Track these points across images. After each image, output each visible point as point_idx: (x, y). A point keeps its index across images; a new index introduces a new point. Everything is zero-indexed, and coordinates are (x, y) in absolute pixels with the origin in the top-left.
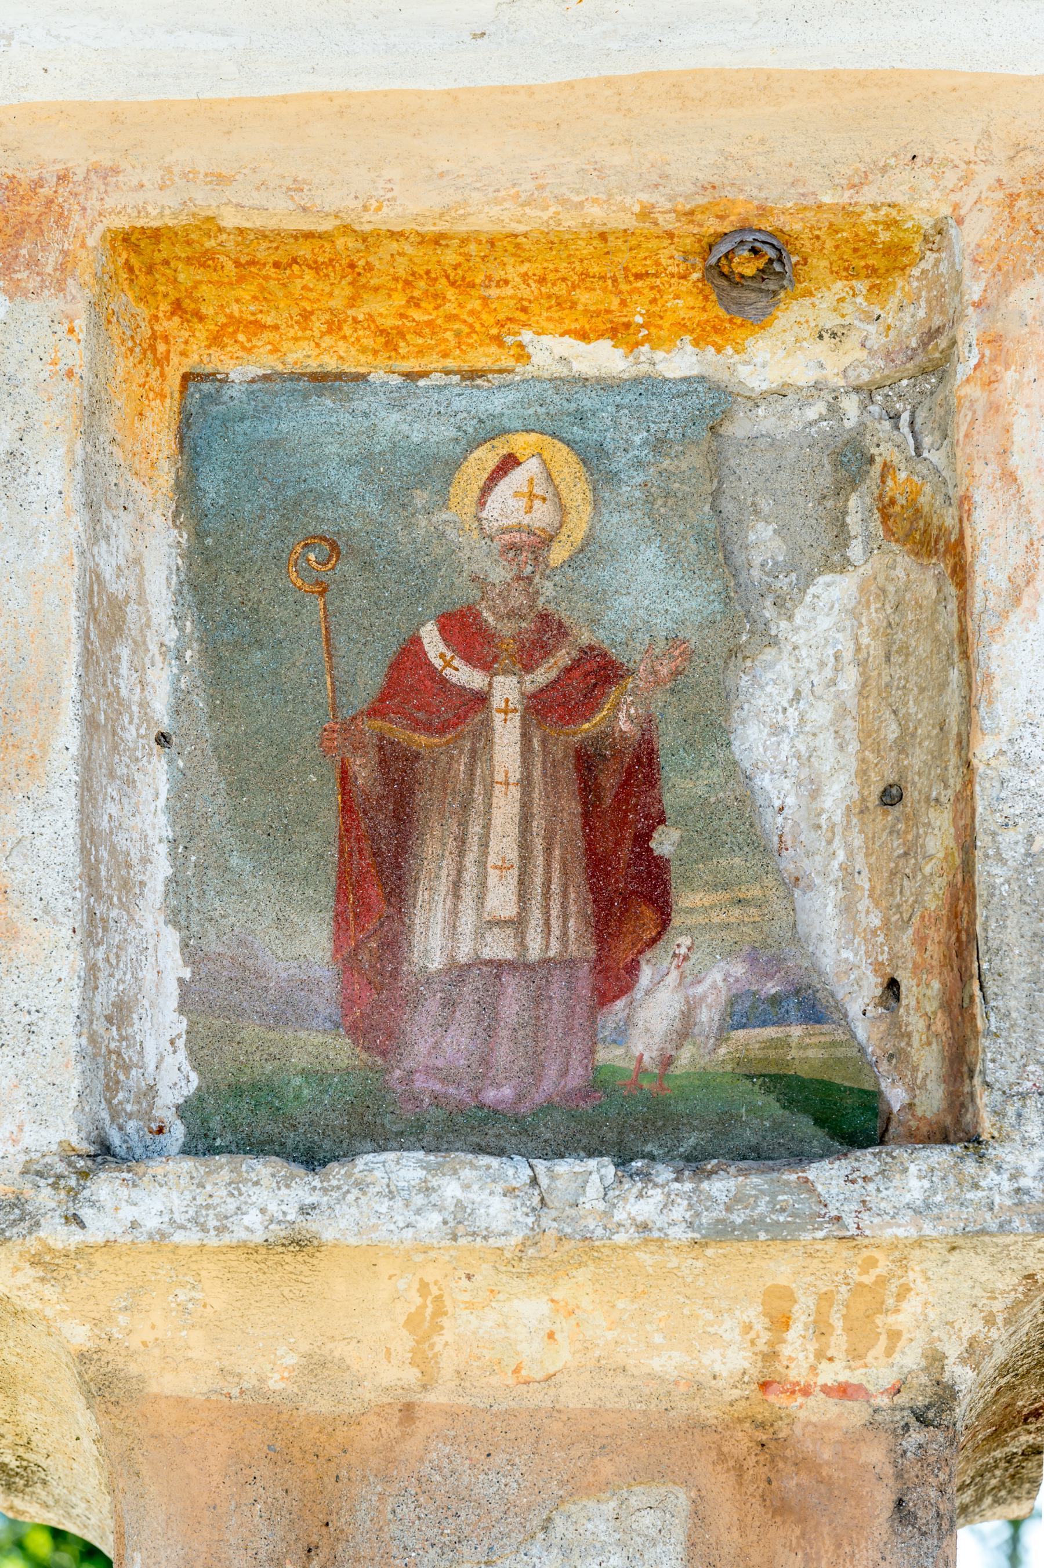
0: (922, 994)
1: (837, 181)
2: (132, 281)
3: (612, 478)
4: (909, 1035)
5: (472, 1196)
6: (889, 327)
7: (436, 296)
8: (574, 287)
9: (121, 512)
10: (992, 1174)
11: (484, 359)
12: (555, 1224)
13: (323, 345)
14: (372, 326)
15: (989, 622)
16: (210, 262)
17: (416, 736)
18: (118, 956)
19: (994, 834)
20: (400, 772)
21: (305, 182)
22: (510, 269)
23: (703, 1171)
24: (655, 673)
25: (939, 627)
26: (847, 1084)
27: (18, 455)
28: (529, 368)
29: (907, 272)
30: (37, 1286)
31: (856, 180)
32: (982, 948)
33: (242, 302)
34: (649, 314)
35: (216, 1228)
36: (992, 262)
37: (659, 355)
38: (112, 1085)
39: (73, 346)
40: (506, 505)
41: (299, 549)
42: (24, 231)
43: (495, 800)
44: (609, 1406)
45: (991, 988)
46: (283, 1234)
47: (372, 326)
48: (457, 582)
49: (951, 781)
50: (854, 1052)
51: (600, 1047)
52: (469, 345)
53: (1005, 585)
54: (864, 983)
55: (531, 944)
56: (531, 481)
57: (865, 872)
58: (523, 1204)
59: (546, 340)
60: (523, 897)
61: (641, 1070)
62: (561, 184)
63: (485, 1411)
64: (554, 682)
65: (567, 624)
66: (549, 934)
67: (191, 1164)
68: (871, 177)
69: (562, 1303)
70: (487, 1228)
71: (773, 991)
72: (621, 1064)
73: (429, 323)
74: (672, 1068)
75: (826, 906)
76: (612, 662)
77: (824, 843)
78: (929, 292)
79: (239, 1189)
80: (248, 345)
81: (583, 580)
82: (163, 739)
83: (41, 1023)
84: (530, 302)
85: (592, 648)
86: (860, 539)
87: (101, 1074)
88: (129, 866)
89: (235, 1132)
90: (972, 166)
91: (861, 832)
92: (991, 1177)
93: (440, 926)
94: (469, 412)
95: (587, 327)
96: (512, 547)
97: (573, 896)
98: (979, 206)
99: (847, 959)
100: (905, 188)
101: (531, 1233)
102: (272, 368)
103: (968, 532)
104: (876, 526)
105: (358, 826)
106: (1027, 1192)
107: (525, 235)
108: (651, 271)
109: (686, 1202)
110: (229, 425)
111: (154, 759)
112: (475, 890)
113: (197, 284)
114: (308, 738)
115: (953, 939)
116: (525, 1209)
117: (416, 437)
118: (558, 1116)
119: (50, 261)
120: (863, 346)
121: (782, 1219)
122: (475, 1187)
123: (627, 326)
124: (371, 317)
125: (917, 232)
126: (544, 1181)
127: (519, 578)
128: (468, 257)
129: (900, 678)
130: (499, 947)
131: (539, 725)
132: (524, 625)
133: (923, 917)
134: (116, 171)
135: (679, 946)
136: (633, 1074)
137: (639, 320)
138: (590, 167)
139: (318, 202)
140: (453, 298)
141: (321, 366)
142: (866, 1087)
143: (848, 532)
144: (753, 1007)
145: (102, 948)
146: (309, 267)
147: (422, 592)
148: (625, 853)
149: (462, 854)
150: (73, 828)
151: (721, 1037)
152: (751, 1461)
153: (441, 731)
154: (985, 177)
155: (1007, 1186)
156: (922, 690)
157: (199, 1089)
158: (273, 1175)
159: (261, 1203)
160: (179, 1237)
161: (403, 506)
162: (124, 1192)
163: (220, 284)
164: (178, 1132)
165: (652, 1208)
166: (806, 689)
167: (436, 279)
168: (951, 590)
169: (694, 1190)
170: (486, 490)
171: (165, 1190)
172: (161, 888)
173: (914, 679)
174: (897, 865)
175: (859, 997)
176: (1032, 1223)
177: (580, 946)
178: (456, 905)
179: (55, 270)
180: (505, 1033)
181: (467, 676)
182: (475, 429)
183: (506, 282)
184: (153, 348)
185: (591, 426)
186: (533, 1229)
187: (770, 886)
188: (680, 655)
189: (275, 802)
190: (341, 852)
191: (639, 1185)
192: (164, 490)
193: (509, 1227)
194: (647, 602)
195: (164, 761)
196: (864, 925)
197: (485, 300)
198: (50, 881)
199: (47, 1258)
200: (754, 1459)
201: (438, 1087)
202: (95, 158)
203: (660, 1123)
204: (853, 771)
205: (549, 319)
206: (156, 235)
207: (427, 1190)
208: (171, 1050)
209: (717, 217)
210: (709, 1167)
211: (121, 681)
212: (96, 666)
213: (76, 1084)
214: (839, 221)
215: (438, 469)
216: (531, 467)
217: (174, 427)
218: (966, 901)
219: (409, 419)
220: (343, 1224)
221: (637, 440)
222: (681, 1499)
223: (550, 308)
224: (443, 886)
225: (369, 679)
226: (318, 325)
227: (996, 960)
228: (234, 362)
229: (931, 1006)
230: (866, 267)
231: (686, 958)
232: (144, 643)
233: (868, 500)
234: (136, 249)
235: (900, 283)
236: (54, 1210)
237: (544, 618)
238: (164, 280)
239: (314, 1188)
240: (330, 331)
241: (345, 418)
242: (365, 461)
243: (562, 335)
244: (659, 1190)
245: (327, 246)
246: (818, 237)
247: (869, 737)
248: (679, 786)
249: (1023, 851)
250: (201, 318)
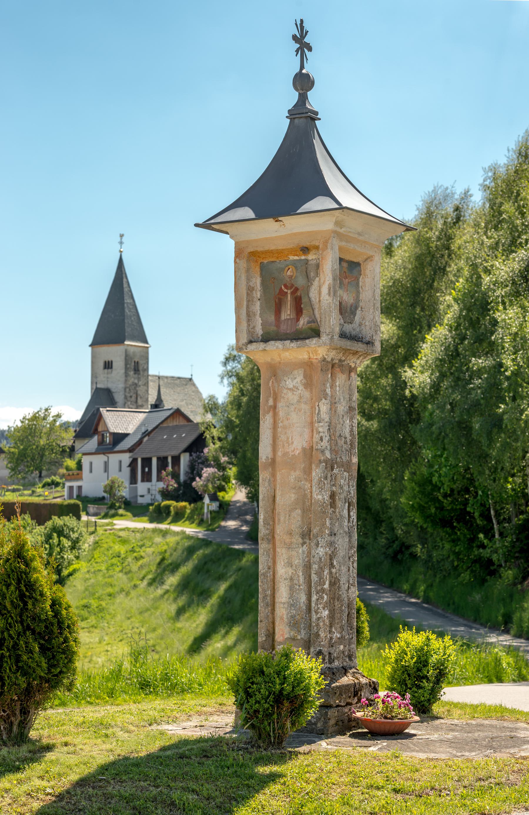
20: (280, 300)
40: (289, 273)
130: (288, 317)
177: (295, 317)
181: (286, 290)
215: (283, 270)
225: (278, 291)
248: (304, 300)
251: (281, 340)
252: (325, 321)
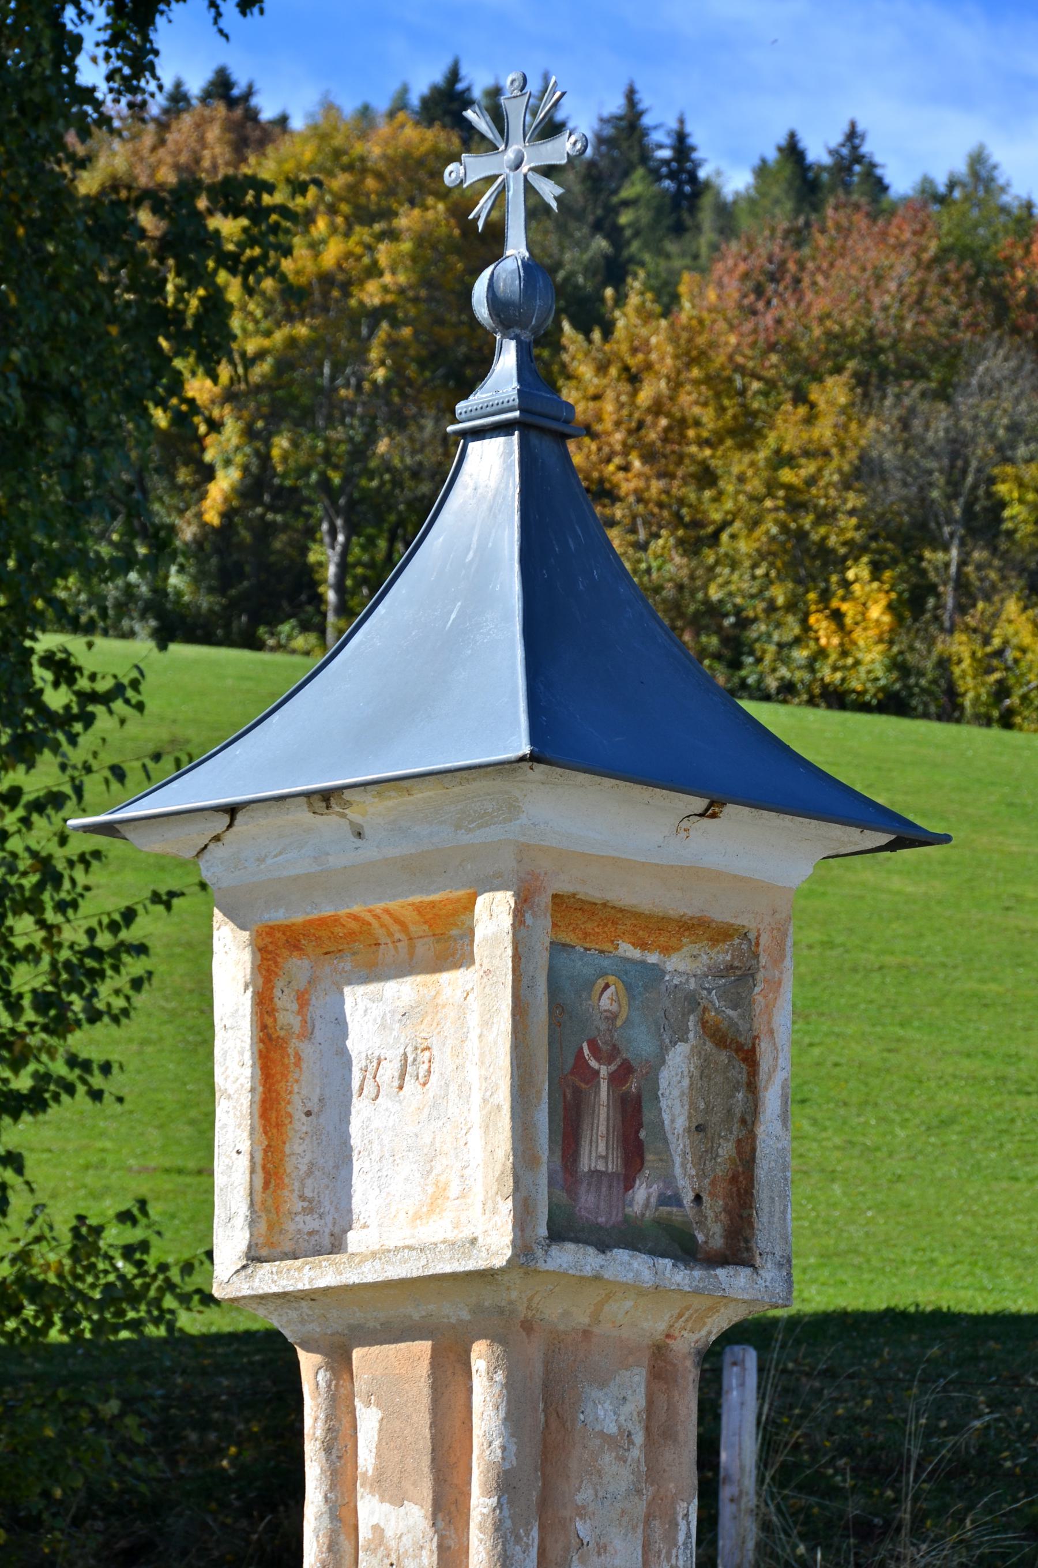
104: (699, 1028)
130: (601, 1167)
177: (620, 1170)
216: (612, 989)
225: (571, 1061)
247: (692, 1105)
248: (647, 1116)
252: (772, 1215)
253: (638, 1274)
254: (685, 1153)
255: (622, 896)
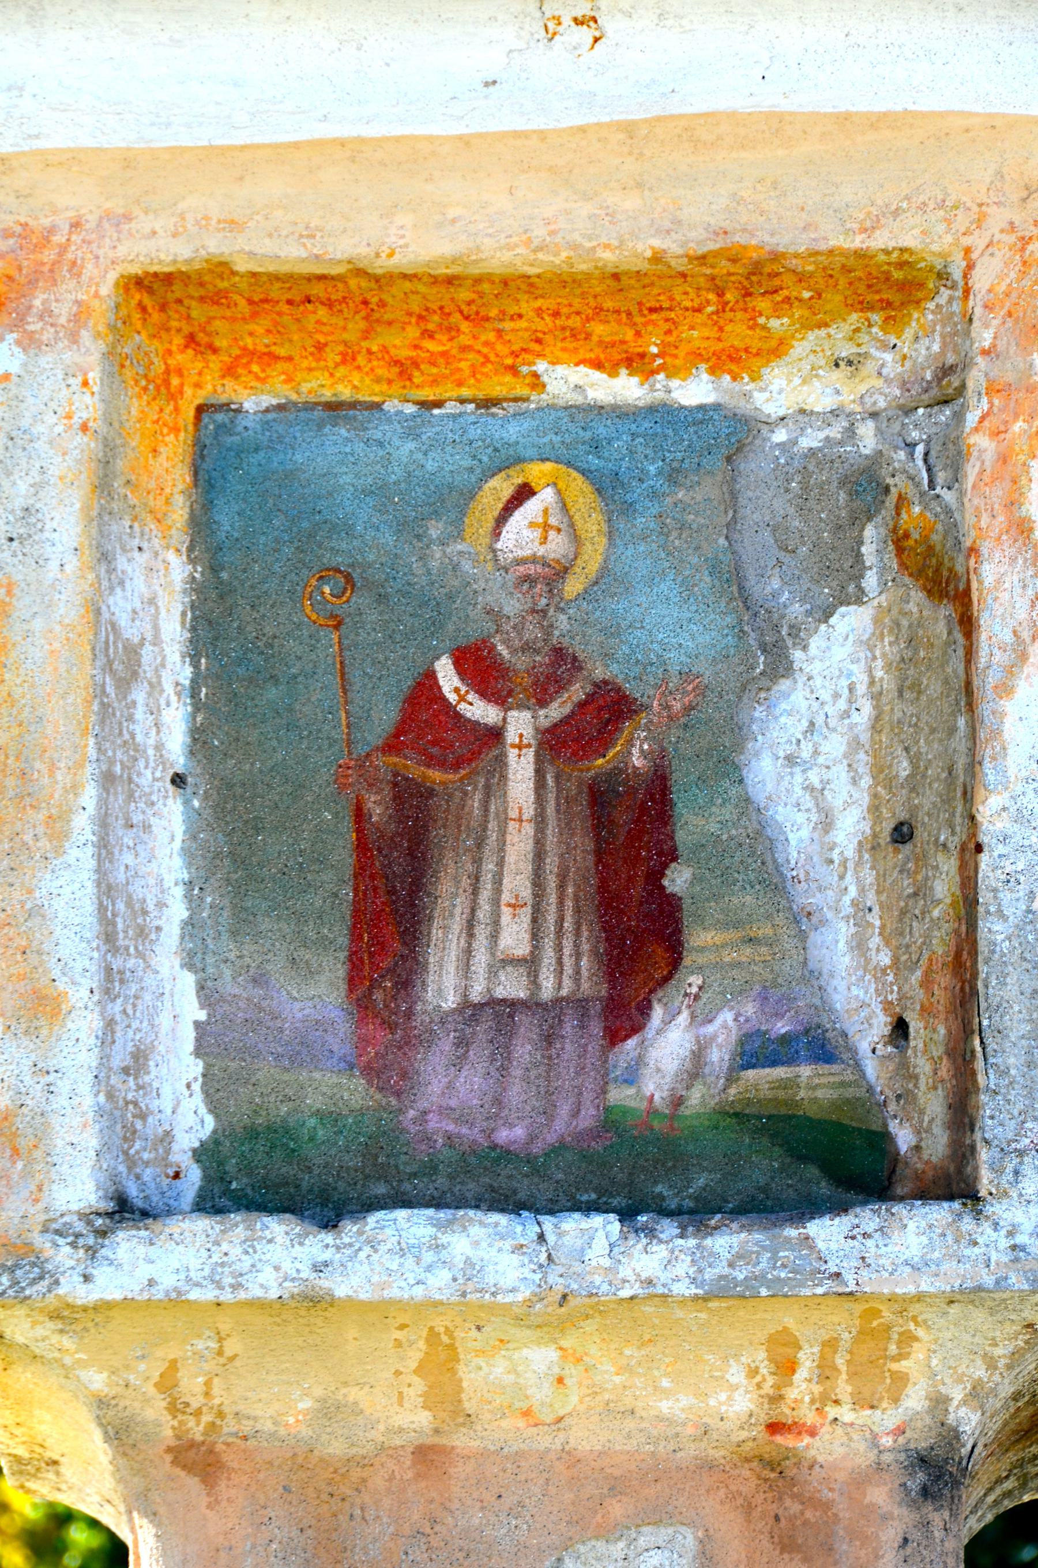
0: (928, 1037)
1: (848, 226)
2: (145, 320)
3: (628, 509)
4: (916, 1077)
5: (481, 1253)
6: (904, 357)
7: (449, 329)
8: (588, 320)
9: (136, 554)
10: (989, 1231)
11: (498, 388)
12: (561, 1280)
13: (338, 375)
14: (387, 357)
15: (993, 678)
16: (223, 301)
17: (430, 772)
18: (134, 1005)
19: (995, 890)
21: (317, 228)
22: (524, 305)
23: (707, 1226)
24: (668, 707)
25: (949, 670)
26: (854, 1124)
27: (33, 511)
28: (544, 396)
29: (923, 304)
30: (55, 1339)
31: (868, 224)
32: (983, 1005)
33: (257, 335)
34: (663, 344)
35: (232, 1286)
36: (1002, 308)
37: (674, 383)
38: (130, 1134)
39: (87, 399)
41: (314, 582)
42: (37, 280)
43: (509, 838)
44: (617, 1448)
45: (992, 1045)
46: (296, 1291)
47: (387, 357)
48: (472, 614)
49: (958, 829)
50: (861, 1093)
51: (611, 1087)
52: (483, 374)
53: (1008, 637)
54: (874, 1021)
55: (545, 983)
56: (546, 511)
57: (876, 909)
58: (531, 1261)
59: (561, 370)
60: (536, 935)
61: (652, 1111)
62: (574, 230)
63: (496, 1453)
64: (568, 717)
65: (581, 658)
66: (561, 973)
67: (207, 1221)
68: (883, 221)
69: (570, 1351)
70: (495, 1285)
71: (783, 1031)
72: (633, 1104)
73: (443, 354)
74: (682, 1108)
75: (837, 942)
76: (625, 697)
77: (836, 878)
78: (944, 326)
79: (253, 1247)
80: (262, 375)
81: (598, 613)
82: (178, 780)
83: (59, 1082)
84: (544, 333)
85: (605, 682)
86: (875, 570)
87: (119, 1126)
88: (145, 913)
89: (250, 1175)
90: (984, 208)
91: (872, 868)
92: (986, 1233)
93: (454, 964)
94: (484, 441)
95: (602, 356)
96: (526, 579)
97: (586, 934)
98: (990, 250)
99: (857, 996)
100: (916, 232)
101: (538, 1290)
102: (286, 397)
103: (974, 585)
105: (373, 864)
106: (1023, 1248)
107: (539, 276)
108: (665, 305)
109: (689, 1258)
110: (243, 455)
111: (170, 801)
112: (489, 928)
113: (210, 320)
114: (325, 775)
115: (958, 987)
116: (532, 1266)
117: (430, 466)
118: (569, 1156)
119: (63, 311)
120: (880, 374)
121: (783, 1275)
122: (484, 1244)
123: (642, 356)
124: (385, 349)
125: (930, 271)
126: (551, 1238)
127: (533, 611)
128: (481, 295)
129: (912, 716)
130: (512, 986)
131: (552, 762)
132: (538, 658)
133: (930, 960)
134: (128, 218)
135: (690, 985)
136: (644, 1114)
137: (654, 350)
138: (602, 212)
139: (331, 249)
140: (467, 331)
141: (335, 395)
142: (874, 1127)
143: (863, 562)
144: (762, 1047)
145: (119, 1001)
146: (323, 303)
147: (436, 626)
148: (637, 891)
149: (475, 892)
150: (90, 888)
151: (730, 1080)
152: (760, 1498)
153: (456, 766)
154: (998, 218)
155: (1004, 1243)
156: (933, 731)
157: (215, 1132)
158: (287, 1233)
159: (275, 1260)
160: (194, 1295)
161: (419, 537)
162: (141, 1250)
163: (233, 319)
164: (194, 1176)
165: (656, 1264)
166: (820, 720)
167: (449, 314)
168: (959, 636)
169: (698, 1246)
170: (502, 520)
171: (181, 1248)
172: (176, 931)
173: (925, 718)
174: (907, 905)
175: (869, 1033)
176: (1028, 1279)
178: (470, 944)
179: (69, 321)
180: (518, 1072)
181: (479, 711)
182: (490, 457)
183: (520, 316)
184: (167, 383)
185: (606, 454)
186: (540, 1286)
187: (781, 924)
188: (694, 690)
189: (290, 841)
190: (356, 890)
191: (644, 1241)
192: (179, 525)
193: (517, 1284)
194: (661, 636)
195: (179, 801)
196: (874, 962)
197: (499, 332)
198: (68, 942)
199: (66, 1313)
200: (762, 1496)
201: (451, 1127)
202: (108, 205)
203: (670, 1164)
204: (865, 807)
205: (564, 349)
206: (168, 279)
207: (437, 1247)
208: (187, 1093)
209: (729, 260)
210: (713, 1222)
211: (136, 727)
212: (109, 715)
213: (94, 1143)
214: (851, 262)
215: (453, 501)
216: (546, 496)
217: (188, 460)
218: (969, 953)
219: (424, 448)
220: (355, 1280)
221: (652, 469)
222: (688, 1539)
223: (564, 339)
224: (457, 925)
225: (384, 715)
226: (332, 356)
227: (996, 1018)
228: (248, 391)
229: (938, 1051)
230: (881, 300)
231: (697, 997)
232: (159, 683)
233: (883, 531)
234: (150, 291)
235: (916, 315)
236: (73, 1268)
237: (559, 653)
238: (177, 316)
239: (327, 1246)
240: (344, 362)
241: (359, 447)
242: (380, 492)
243: (577, 364)
244: (663, 1246)
245: (340, 286)
246: (831, 276)
247: (880, 771)
248: (693, 822)
249: (1024, 907)
250: (215, 351)
251: (510, 1203)
253: (471, 1269)
254: (861, 909)
255: (413, 238)
